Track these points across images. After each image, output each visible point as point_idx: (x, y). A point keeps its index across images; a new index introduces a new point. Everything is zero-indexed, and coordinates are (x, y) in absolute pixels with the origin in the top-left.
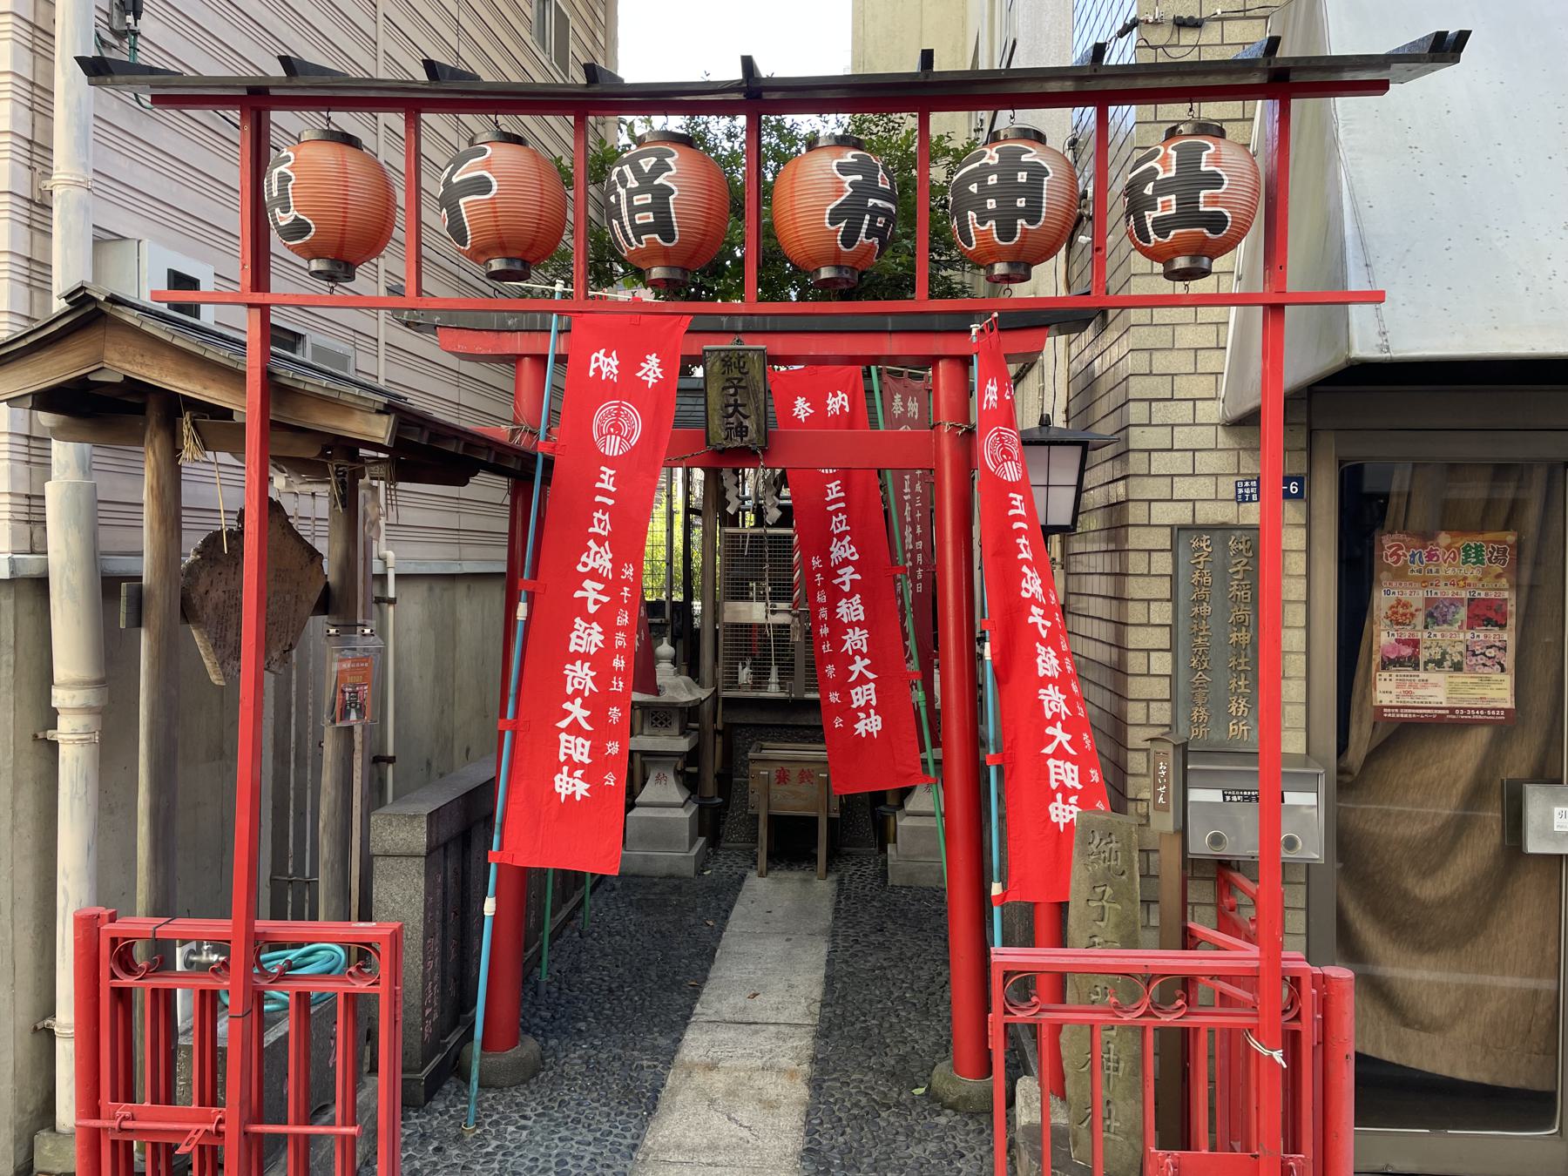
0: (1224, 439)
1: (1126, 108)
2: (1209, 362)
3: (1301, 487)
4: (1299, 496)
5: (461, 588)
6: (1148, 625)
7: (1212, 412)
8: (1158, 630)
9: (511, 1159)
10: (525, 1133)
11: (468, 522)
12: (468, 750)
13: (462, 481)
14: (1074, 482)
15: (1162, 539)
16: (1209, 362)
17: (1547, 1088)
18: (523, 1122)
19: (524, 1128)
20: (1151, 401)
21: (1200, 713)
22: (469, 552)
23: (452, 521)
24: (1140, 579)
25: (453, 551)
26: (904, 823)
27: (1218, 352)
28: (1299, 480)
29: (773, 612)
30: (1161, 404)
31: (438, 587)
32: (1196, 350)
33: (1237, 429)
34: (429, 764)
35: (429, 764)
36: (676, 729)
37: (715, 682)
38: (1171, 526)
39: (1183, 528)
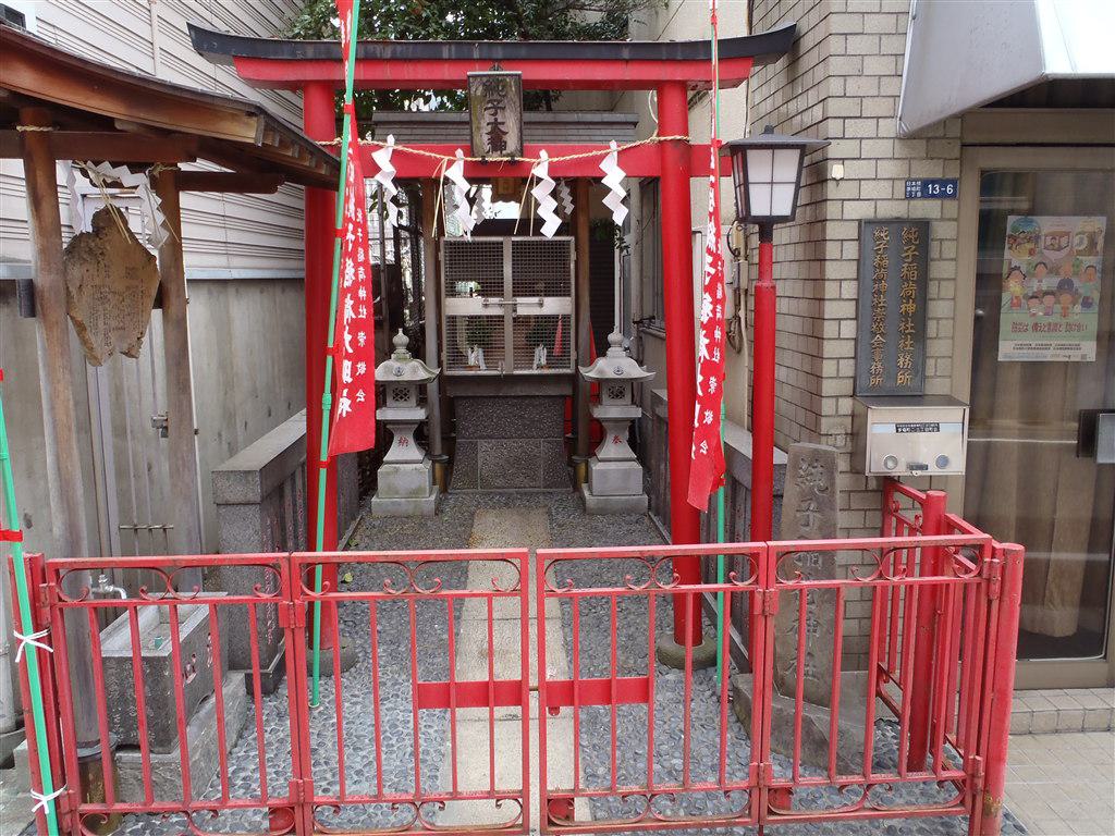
0: (900, 151)
1: (24, 189)
2: (889, 87)
3: (955, 188)
4: (953, 196)
5: (231, 290)
6: (840, 299)
7: (889, 128)
8: (847, 303)
9: (354, 727)
10: (358, 707)
11: (233, 237)
12: (246, 423)
13: (271, 190)
14: (794, 179)
15: (852, 231)
16: (889, 87)
17: (423, 712)
18: (355, 699)
19: (355, 704)
20: (845, 118)
21: (877, 366)
22: (236, 261)
23: (219, 235)
24: (835, 263)
25: (223, 260)
26: (596, 467)
27: (896, 79)
28: (954, 182)
29: (486, 306)
30: (853, 121)
31: (214, 288)
32: (880, 76)
33: (909, 142)
34: (220, 435)
35: (220, 435)
36: (413, 401)
37: (440, 364)
38: (860, 221)
39: (869, 222)
